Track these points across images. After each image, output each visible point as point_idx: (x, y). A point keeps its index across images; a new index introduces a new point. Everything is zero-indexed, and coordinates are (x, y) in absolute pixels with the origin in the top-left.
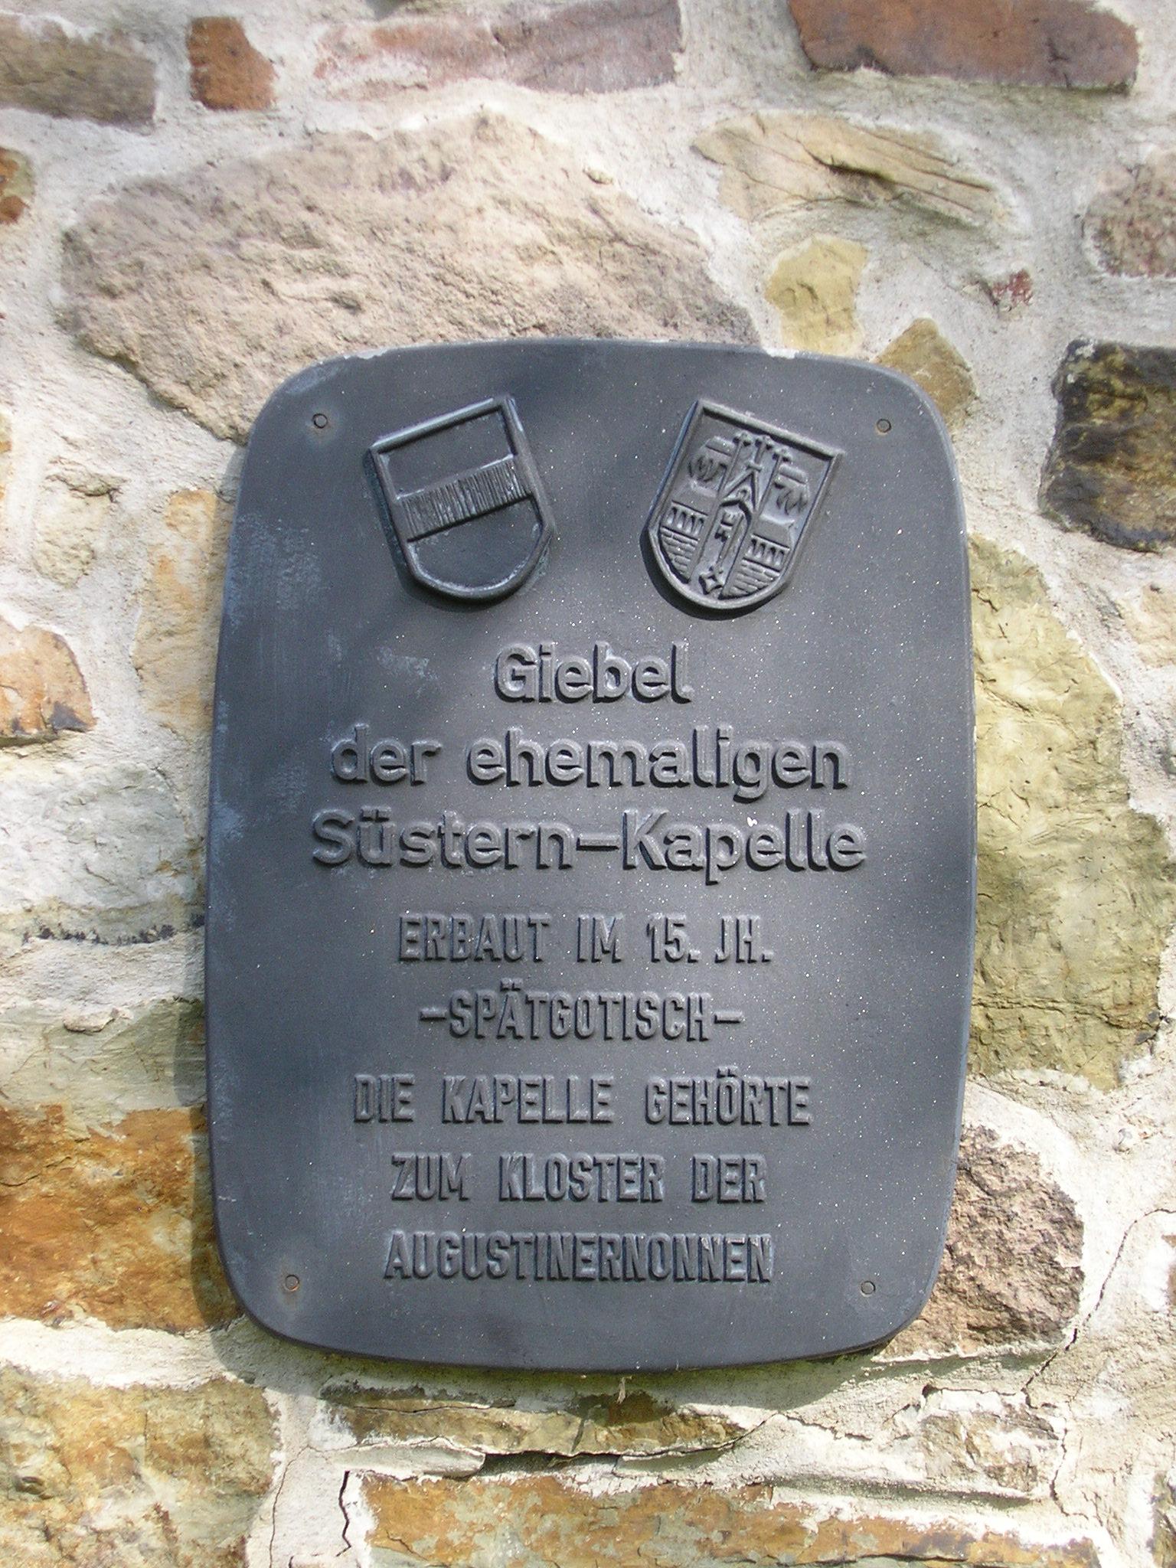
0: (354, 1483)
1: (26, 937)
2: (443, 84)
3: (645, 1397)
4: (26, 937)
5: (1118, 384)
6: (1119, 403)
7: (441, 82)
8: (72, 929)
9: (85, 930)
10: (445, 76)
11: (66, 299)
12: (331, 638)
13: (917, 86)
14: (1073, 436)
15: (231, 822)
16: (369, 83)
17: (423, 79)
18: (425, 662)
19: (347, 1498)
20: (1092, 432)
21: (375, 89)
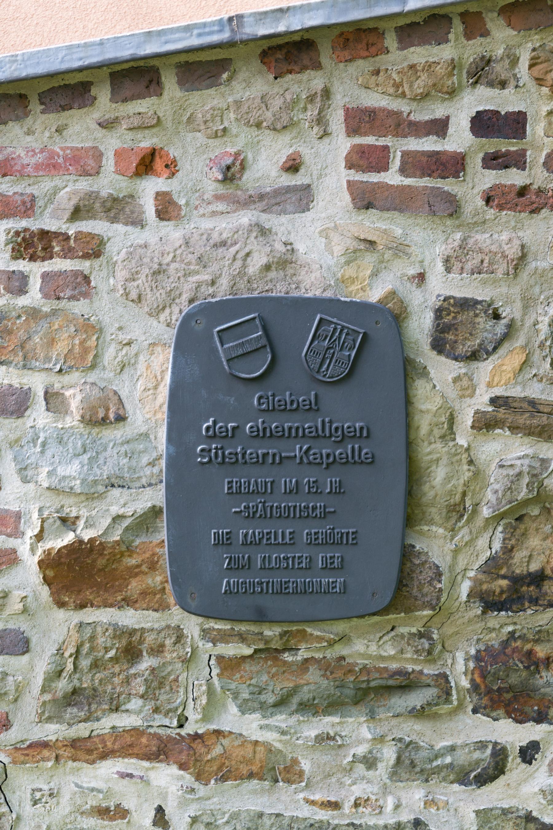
0: (213, 658)
1: (106, 487)
2: (280, 215)
3: (304, 631)
4: (106, 487)
5: (452, 309)
6: (453, 315)
7: (235, 211)
8: (121, 484)
9: (125, 484)
10: (236, 209)
11: (126, 564)
12: (203, 391)
13: (386, 215)
14: (438, 325)
15: (172, 449)
16: (213, 212)
17: (229, 210)
18: (233, 398)
19: (211, 663)
20: (444, 323)
21: (214, 214)
